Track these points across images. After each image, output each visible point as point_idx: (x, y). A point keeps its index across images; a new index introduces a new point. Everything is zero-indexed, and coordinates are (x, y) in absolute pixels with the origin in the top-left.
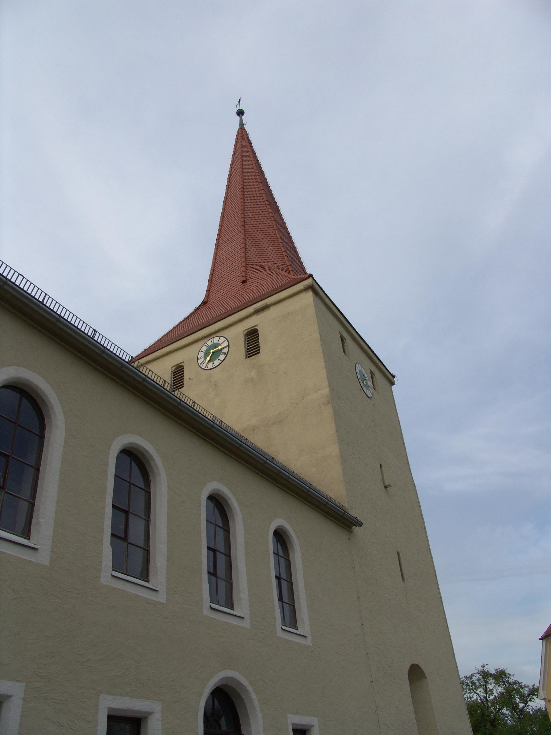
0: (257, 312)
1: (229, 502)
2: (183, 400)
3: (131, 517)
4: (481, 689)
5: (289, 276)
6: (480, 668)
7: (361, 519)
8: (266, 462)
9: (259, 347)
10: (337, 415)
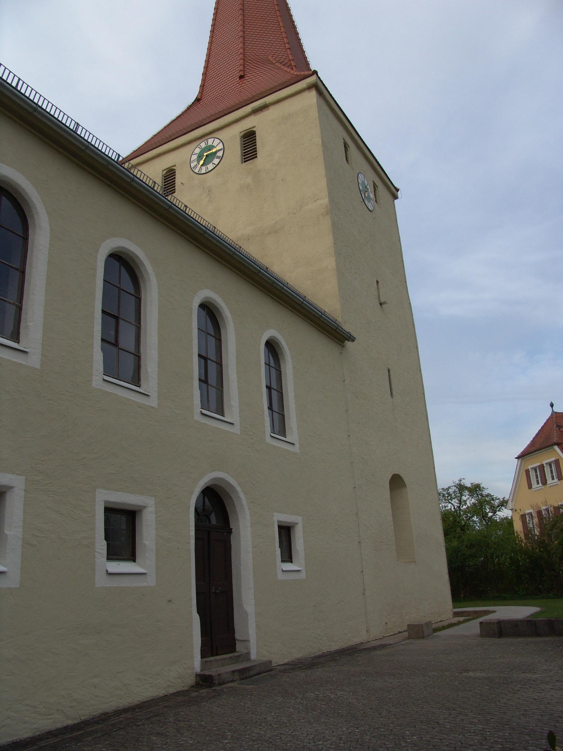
0: (255, 111)
1: (221, 310)
2: (174, 203)
3: (121, 322)
4: (456, 500)
5: (292, 72)
6: (457, 482)
7: (353, 334)
8: (259, 272)
9: (256, 151)
10: (336, 228)
